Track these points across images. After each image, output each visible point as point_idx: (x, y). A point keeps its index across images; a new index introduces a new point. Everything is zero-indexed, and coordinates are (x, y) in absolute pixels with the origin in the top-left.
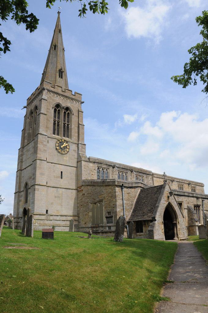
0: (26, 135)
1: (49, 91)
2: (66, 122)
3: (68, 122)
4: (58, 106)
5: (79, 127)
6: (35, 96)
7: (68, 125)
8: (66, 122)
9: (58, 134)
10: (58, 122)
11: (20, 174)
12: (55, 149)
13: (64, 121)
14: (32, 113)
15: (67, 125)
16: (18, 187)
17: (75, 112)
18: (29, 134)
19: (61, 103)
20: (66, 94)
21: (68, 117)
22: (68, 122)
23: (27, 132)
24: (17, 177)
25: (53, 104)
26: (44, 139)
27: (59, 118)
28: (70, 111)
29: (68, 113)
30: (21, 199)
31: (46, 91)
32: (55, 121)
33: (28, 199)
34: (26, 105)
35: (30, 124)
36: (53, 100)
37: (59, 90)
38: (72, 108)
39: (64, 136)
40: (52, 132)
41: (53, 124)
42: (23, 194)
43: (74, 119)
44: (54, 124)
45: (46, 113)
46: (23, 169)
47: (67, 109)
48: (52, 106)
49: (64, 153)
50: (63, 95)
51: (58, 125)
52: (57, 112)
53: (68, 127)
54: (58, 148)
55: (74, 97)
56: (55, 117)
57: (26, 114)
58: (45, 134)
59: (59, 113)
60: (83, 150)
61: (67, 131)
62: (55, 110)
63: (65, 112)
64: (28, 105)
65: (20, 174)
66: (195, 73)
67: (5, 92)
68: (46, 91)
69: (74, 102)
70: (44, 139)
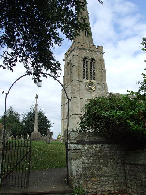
0: (66, 80)
1: (78, 48)
2: (92, 69)
3: (94, 68)
4: (86, 58)
5: (101, 72)
6: (70, 52)
7: (94, 71)
8: (92, 69)
9: (87, 79)
10: (87, 70)
11: (64, 107)
12: (85, 89)
13: (91, 68)
14: (68, 64)
15: (93, 70)
16: (63, 116)
17: (97, 60)
18: (68, 79)
19: (88, 55)
20: (91, 49)
21: (94, 66)
22: (94, 68)
23: (66, 78)
24: (62, 109)
25: (83, 57)
26: (77, 83)
27: (87, 67)
28: (95, 60)
29: (94, 62)
30: (65, 124)
31: (77, 49)
32: (84, 70)
33: (70, 124)
34: (64, 59)
35: (68, 71)
36: (82, 55)
37: (86, 47)
38: (96, 58)
39: (91, 79)
40: (82, 77)
41: (83, 72)
42: (66, 120)
43: (97, 66)
44: (84, 72)
45: (77, 65)
46: (65, 103)
47: (93, 59)
48: (82, 59)
49: (92, 91)
50: (88, 50)
51: (87, 72)
52: (85, 62)
53: (94, 73)
54: (87, 88)
55: (97, 50)
56: (84, 66)
57: (65, 65)
58: (78, 80)
59: (87, 63)
60: (106, 88)
61: (93, 77)
62: (84, 61)
63: (91, 62)
64: (65, 58)
65: (64, 107)
66: (60, 39)
67: (11, 71)
68: (77, 49)
69: (98, 53)
70: (77, 83)
